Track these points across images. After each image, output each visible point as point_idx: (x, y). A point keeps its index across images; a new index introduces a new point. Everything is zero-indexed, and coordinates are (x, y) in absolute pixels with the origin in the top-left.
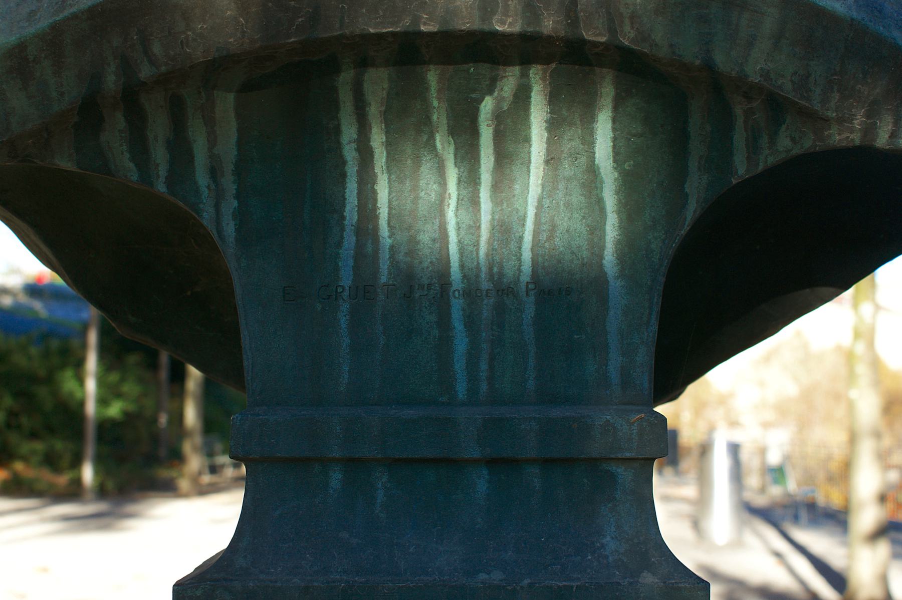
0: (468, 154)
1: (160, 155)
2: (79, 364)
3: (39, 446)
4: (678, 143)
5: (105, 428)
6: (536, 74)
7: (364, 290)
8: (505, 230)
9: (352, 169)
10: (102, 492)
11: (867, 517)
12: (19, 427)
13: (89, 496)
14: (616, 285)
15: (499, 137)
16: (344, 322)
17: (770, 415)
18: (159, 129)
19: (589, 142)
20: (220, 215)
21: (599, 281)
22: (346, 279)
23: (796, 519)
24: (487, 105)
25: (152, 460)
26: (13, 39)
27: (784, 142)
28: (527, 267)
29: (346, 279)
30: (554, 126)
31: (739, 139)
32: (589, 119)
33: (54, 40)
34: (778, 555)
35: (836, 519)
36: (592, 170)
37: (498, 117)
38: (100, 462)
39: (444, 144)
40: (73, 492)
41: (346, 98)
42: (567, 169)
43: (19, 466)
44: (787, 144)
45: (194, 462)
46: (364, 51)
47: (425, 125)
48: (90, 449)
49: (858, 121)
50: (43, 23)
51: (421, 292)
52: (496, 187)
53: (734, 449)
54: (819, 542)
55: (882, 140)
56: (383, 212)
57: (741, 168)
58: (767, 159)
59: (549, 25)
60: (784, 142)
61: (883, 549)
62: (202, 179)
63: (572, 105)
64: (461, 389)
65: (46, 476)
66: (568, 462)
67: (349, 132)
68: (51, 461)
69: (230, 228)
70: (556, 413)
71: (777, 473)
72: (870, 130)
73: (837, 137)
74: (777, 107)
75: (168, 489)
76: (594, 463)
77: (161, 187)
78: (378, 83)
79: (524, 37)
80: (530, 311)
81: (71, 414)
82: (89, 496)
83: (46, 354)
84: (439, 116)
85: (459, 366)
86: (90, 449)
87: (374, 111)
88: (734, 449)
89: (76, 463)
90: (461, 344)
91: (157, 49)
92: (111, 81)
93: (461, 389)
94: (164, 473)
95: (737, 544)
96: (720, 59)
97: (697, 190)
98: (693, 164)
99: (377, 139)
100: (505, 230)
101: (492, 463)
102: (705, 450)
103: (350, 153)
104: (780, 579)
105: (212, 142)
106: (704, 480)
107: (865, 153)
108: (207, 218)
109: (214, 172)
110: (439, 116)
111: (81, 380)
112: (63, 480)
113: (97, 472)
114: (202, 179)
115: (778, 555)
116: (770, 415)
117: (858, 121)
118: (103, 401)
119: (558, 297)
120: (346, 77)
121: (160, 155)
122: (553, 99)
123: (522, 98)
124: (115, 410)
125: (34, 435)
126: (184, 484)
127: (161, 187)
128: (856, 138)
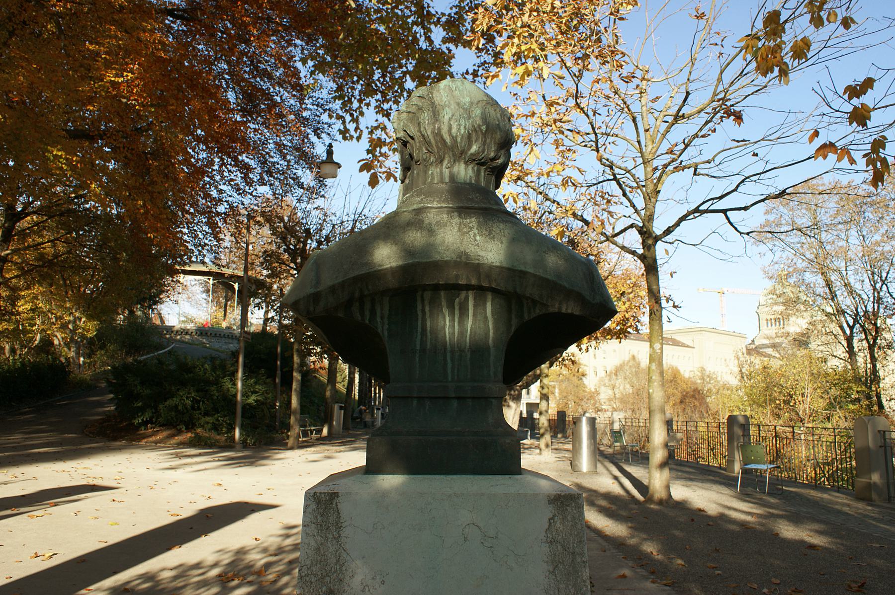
0: (452, 314)
1: (367, 313)
2: (234, 374)
3: (208, 419)
4: (509, 311)
5: (246, 408)
6: (470, 292)
7: (423, 350)
8: (462, 333)
9: (420, 317)
10: (244, 445)
11: (658, 455)
12: (199, 409)
13: (238, 447)
14: (492, 350)
15: (460, 309)
16: (417, 359)
17: (617, 404)
18: (368, 306)
19: (485, 310)
20: (382, 327)
21: (488, 349)
22: (418, 347)
23: (627, 461)
24: (457, 300)
25: (271, 428)
26: (331, 284)
27: (537, 311)
28: (468, 344)
29: (418, 347)
30: (475, 306)
31: (525, 310)
32: (485, 304)
33: (342, 285)
34: (616, 478)
35: (643, 458)
36: (486, 318)
37: (460, 304)
38: (242, 428)
39: (446, 312)
40: (229, 445)
41: (419, 299)
42: (479, 317)
43: (199, 430)
44: (538, 311)
45: (296, 430)
46: (425, 288)
47: (440, 305)
48: (239, 420)
49: (557, 305)
50: (341, 280)
51: (439, 350)
52: (459, 322)
53: (592, 422)
54: (636, 471)
55: (564, 310)
56: (429, 329)
57: (526, 317)
58: (533, 315)
59: (474, 282)
60: (537, 311)
61: (666, 472)
62: (379, 319)
63: (480, 303)
64: (450, 379)
65: (214, 436)
66: (479, 398)
67: (419, 307)
68: (216, 428)
69: (386, 333)
70: (476, 384)
71: (617, 435)
72: (560, 308)
73: (551, 310)
74: (534, 302)
75: (283, 445)
76: (486, 398)
77: (367, 322)
78: (428, 295)
79: (466, 285)
80: (469, 356)
81: (229, 401)
82: (238, 447)
83: (214, 369)
84: (444, 303)
85: (449, 371)
86: (239, 420)
87: (426, 302)
88: (592, 422)
89: (231, 429)
90: (450, 365)
91: (370, 287)
92: (357, 295)
93: (450, 379)
94: (278, 436)
95: (594, 472)
96: (518, 290)
97: (515, 322)
98: (513, 317)
99: (427, 309)
100: (462, 333)
101: (459, 398)
102: (576, 422)
103: (419, 313)
104: (616, 489)
105: (382, 310)
106: (576, 440)
107: (559, 314)
108: (380, 330)
109: (382, 318)
110: (444, 303)
111: (235, 384)
112: (223, 438)
113: (241, 434)
114: (379, 319)
115: (616, 478)
116: (617, 404)
117: (557, 305)
118: (244, 394)
119: (478, 350)
120: (419, 293)
121: (367, 313)
122: (475, 299)
123: (467, 298)
124: (252, 400)
125: (206, 414)
126: (291, 442)
127: (367, 322)
128: (556, 310)
